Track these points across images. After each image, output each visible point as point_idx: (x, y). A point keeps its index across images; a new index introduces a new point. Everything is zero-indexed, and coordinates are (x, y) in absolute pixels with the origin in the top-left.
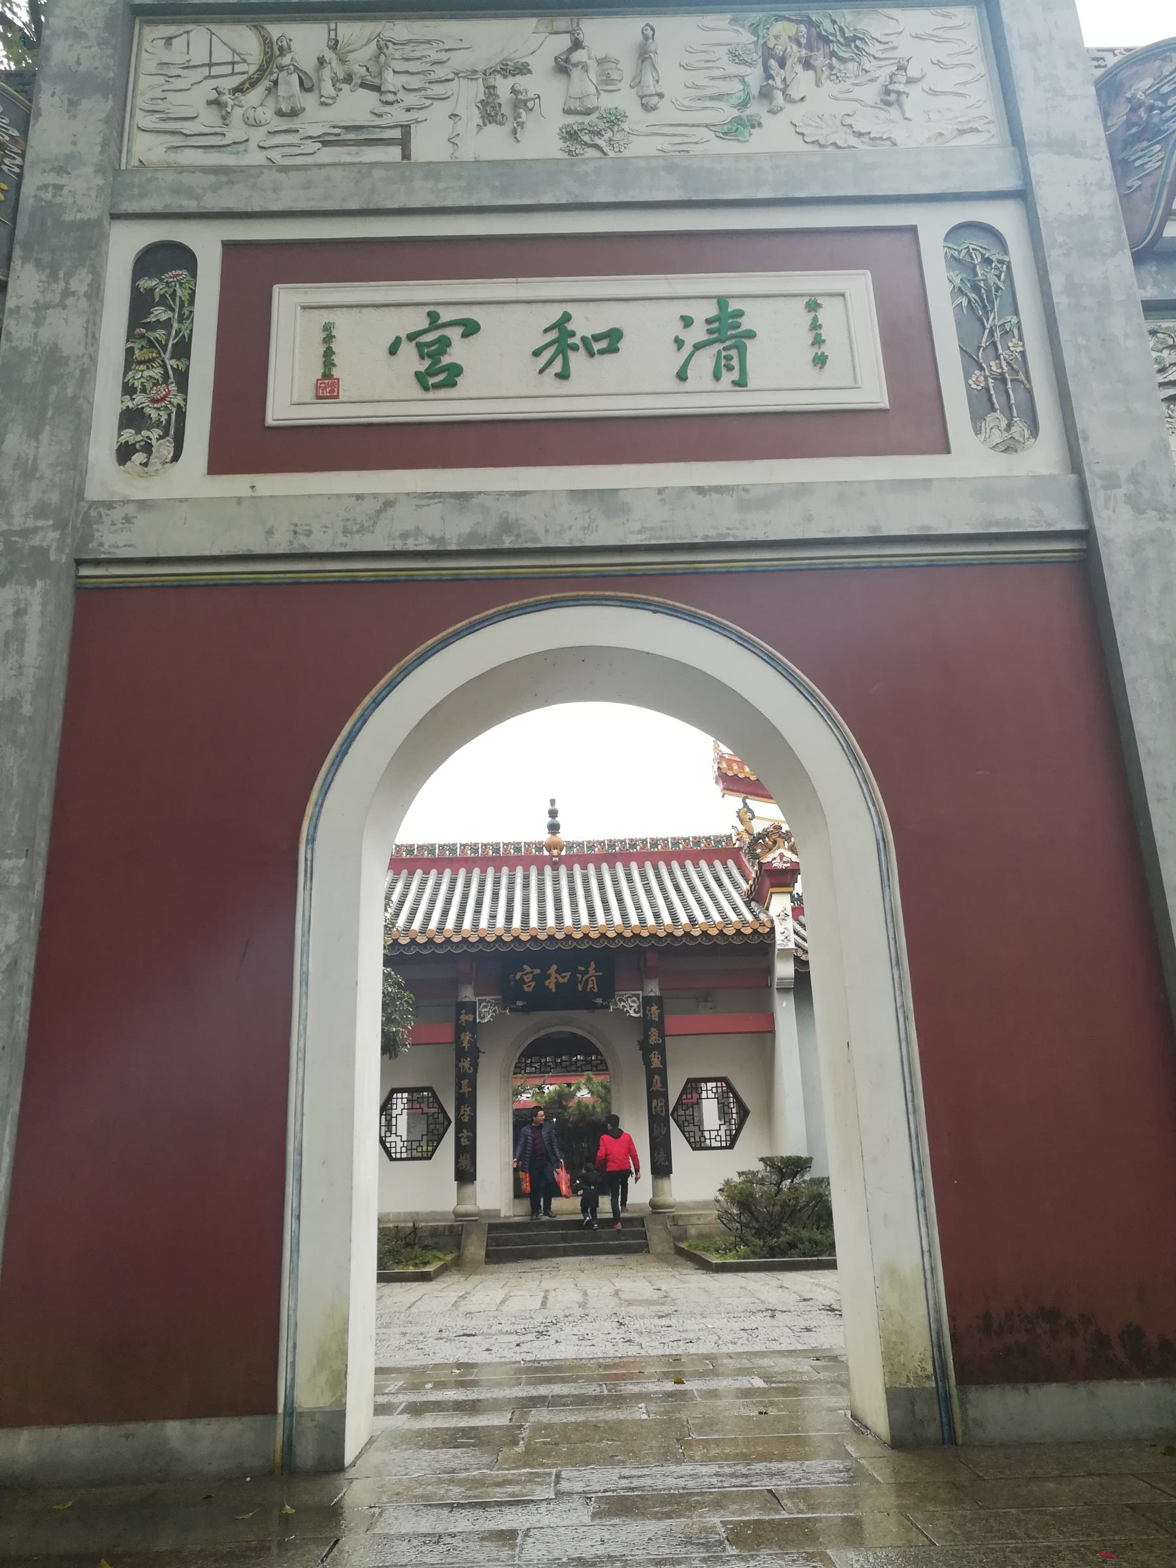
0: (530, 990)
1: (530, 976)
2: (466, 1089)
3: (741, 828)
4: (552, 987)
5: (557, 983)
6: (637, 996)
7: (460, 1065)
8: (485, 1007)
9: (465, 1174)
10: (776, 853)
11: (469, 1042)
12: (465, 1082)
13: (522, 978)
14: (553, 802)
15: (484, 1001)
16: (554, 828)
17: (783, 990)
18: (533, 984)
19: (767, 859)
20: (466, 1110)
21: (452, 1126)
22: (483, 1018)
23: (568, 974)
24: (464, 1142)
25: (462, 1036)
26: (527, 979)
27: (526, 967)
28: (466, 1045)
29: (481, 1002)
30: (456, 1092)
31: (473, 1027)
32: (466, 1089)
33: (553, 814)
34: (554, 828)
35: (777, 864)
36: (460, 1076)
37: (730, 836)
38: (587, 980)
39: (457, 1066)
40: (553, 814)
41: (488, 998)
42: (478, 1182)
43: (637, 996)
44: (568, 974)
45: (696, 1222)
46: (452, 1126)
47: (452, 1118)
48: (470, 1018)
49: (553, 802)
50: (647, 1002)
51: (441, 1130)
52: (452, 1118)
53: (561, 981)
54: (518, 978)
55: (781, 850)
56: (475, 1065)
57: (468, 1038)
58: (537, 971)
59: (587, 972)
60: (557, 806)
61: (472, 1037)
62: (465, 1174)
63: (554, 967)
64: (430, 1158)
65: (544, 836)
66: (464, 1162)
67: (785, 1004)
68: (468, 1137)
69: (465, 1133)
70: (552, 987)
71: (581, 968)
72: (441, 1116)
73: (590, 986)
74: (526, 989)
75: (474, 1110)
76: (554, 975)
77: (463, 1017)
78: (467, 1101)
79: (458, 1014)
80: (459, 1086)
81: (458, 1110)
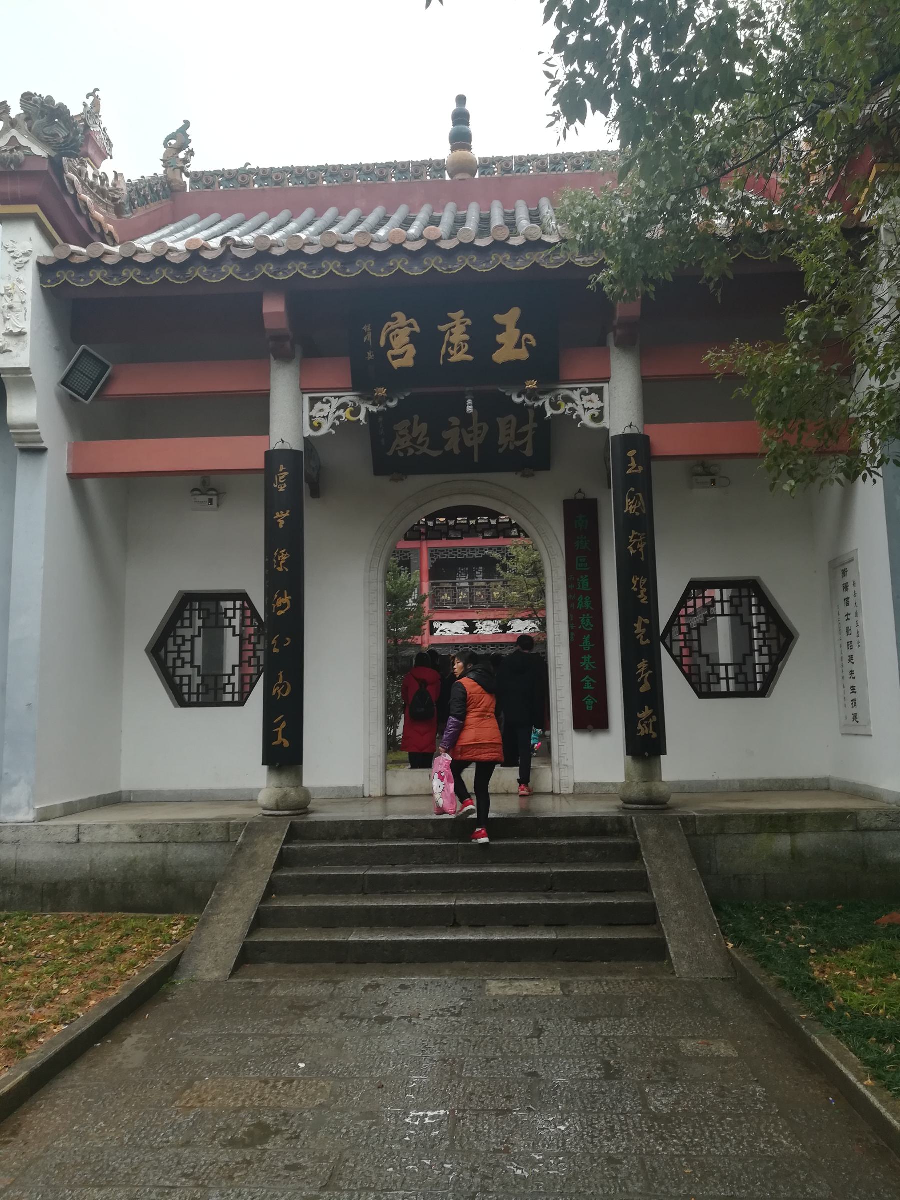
9: (283, 750)
14: (461, 100)
16: (461, 139)
33: (461, 118)
34: (461, 139)
40: (461, 118)
49: (461, 100)
60: (468, 107)
62: (283, 750)
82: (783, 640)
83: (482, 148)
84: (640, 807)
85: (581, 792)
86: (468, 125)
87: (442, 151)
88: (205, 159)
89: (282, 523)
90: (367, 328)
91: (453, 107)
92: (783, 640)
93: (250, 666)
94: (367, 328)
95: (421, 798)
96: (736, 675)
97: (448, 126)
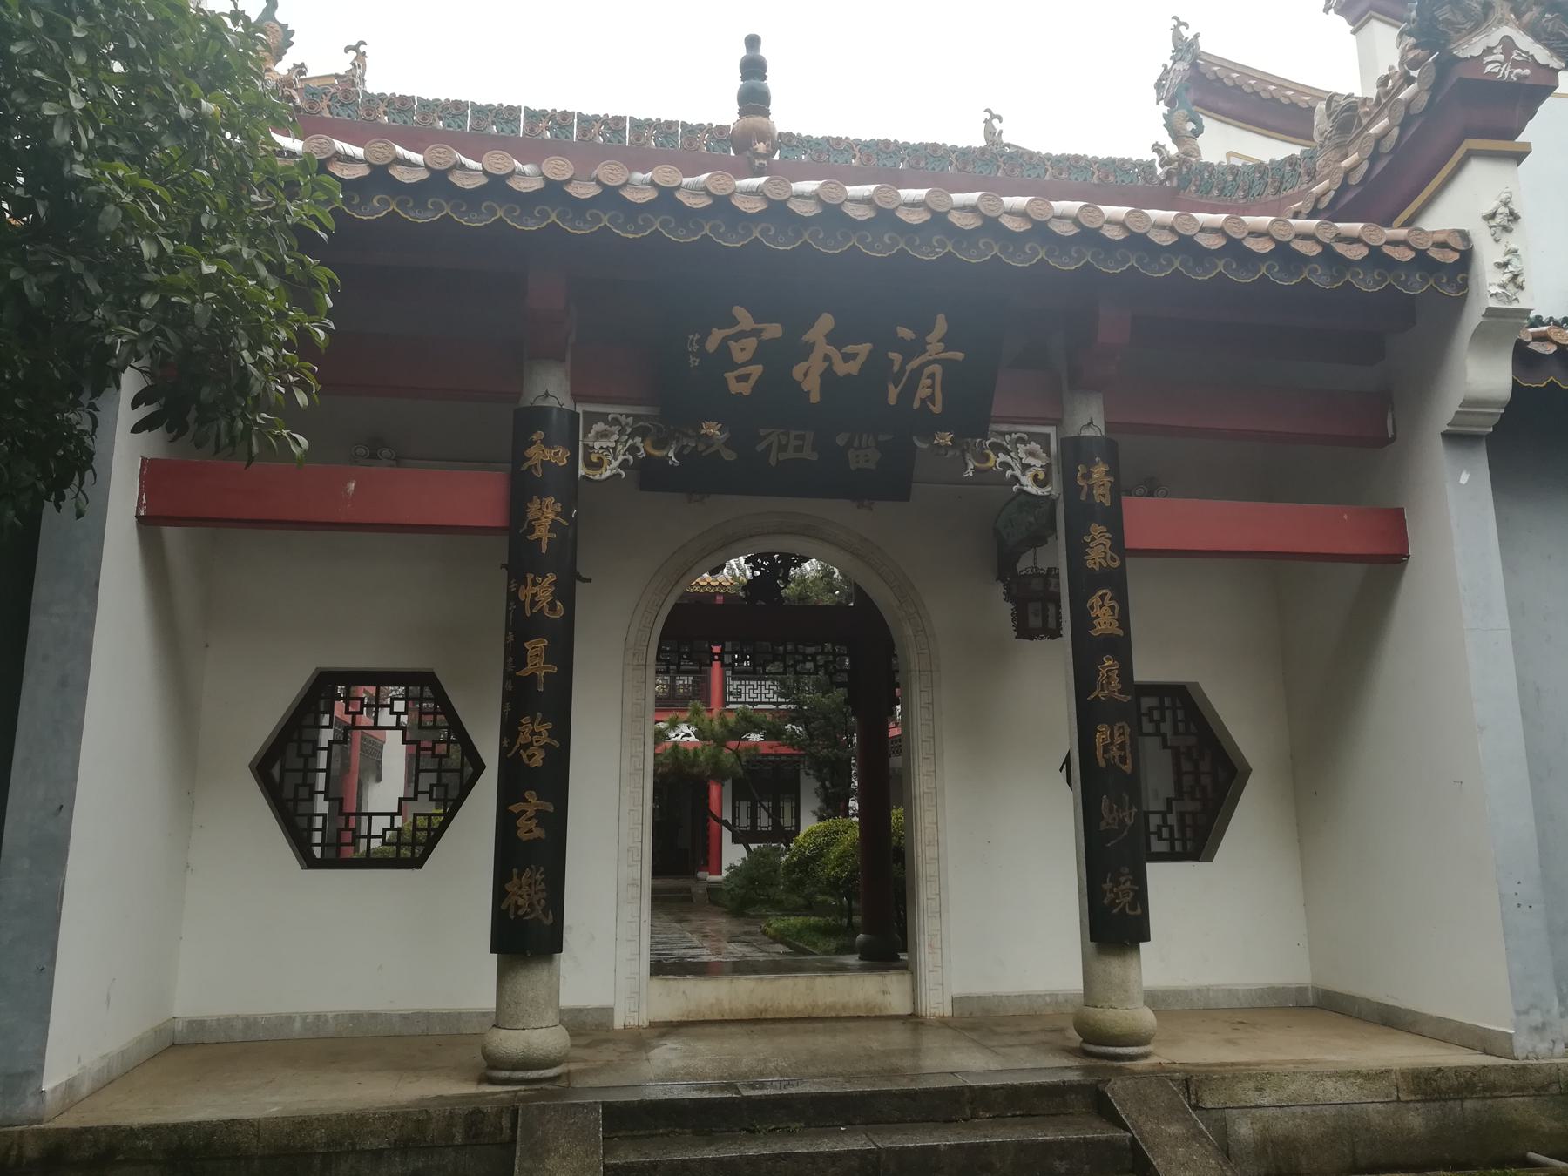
0: (745, 389)
1: (751, 344)
2: (538, 665)
3: (1173, 150)
4: (812, 386)
5: (828, 377)
6: (1044, 440)
7: (525, 594)
8: (603, 435)
9: (527, 931)
10: (1495, 36)
11: (554, 526)
12: (537, 646)
13: (724, 346)
14: (753, 42)
15: (603, 417)
16: (754, 99)
17: (1456, 438)
18: (756, 370)
19: (1472, 48)
20: (537, 730)
21: (486, 790)
22: (598, 465)
23: (864, 349)
24: (529, 830)
25: (533, 507)
26: (742, 351)
27: (740, 312)
28: (543, 533)
29: (592, 418)
30: (508, 676)
31: (570, 488)
32: (538, 665)
33: (753, 68)
34: (754, 99)
35: (1495, 67)
36: (521, 625)
37: (1150, 164)
38: (918, 371)
39: (513, 597)
40: (753, 68)
41: (613, 410)
42: (564, 960)
43: (1044, 440)
44: (864, 349)
45: (1252, 1097)
46: (486, 790)
47: (489, 748)
48: (560, 456)
49: (753, 42)
50: (1074, 452)
51: (454, 794)
52: (489, 748)
53: (841, 368)
54: (712, 345)
55: (1506, 30)
56: (566, 593)
57: (550, 515)
58: (773, 330)
59: (917, 347)
60: (764, 51)
61: (565, 514)
62: (527, 931)
63: (826, 322)
64: (417, 863)
65: (724, 112)
66: (525, 892)
67: (1464, 478)
68: (540, 814)
69: (532, 802)
70: (812, 386)
71: (905, 333)
72: (456, 751)
73: (923, 392)
74: (735, 387)
75: (562, 732)
76: (823, 348)
77: (537, 454)
78: (540, 705)
79: (521, 443)
80: (515, 655)
81: (509, 730)
82: (469, 770)
83: (785, 117)
84: (1112, 1050)
85: (978, 1021)
86: (764, 78)
87: (724, 112)
88: (377, 83)
89: (892, 355)
90: (757, 162)
91: (742, 52)
92: (469, 770)
93: (448, 755)
94: (757, 162)
95: (733, 1029)
96: (315, 755)
97: (735, 82)
